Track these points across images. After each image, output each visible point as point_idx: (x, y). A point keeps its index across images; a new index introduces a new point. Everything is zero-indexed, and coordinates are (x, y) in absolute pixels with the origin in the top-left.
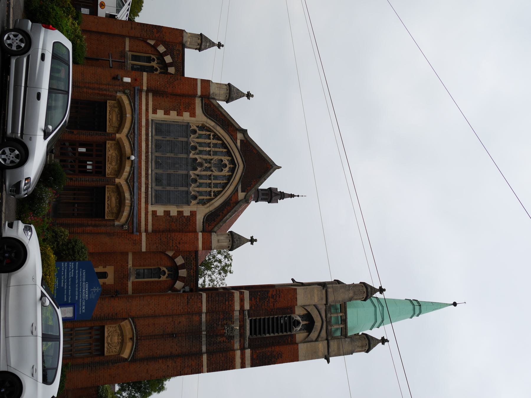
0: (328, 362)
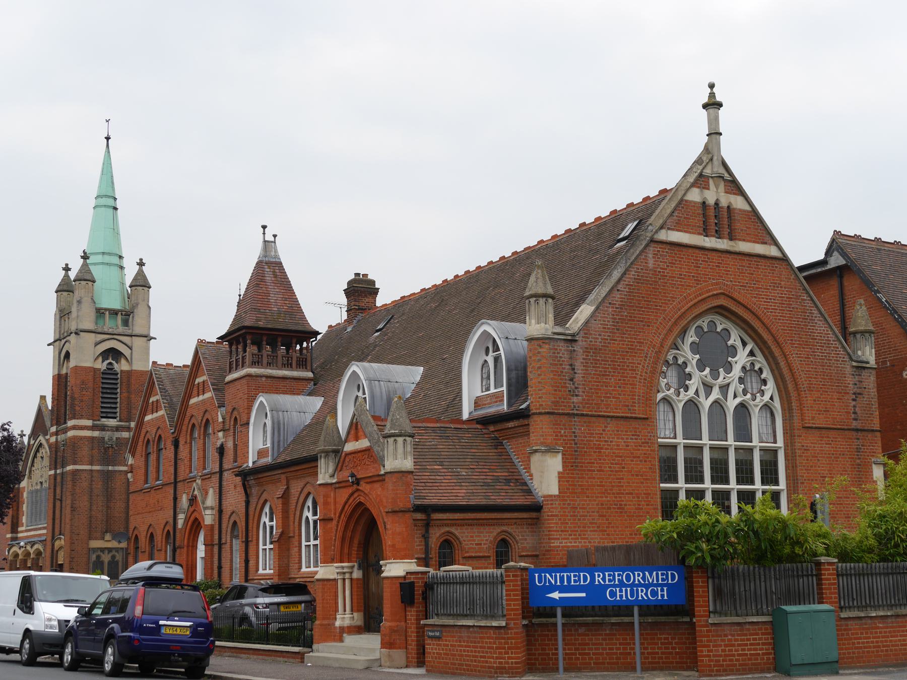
0: (155, 339)
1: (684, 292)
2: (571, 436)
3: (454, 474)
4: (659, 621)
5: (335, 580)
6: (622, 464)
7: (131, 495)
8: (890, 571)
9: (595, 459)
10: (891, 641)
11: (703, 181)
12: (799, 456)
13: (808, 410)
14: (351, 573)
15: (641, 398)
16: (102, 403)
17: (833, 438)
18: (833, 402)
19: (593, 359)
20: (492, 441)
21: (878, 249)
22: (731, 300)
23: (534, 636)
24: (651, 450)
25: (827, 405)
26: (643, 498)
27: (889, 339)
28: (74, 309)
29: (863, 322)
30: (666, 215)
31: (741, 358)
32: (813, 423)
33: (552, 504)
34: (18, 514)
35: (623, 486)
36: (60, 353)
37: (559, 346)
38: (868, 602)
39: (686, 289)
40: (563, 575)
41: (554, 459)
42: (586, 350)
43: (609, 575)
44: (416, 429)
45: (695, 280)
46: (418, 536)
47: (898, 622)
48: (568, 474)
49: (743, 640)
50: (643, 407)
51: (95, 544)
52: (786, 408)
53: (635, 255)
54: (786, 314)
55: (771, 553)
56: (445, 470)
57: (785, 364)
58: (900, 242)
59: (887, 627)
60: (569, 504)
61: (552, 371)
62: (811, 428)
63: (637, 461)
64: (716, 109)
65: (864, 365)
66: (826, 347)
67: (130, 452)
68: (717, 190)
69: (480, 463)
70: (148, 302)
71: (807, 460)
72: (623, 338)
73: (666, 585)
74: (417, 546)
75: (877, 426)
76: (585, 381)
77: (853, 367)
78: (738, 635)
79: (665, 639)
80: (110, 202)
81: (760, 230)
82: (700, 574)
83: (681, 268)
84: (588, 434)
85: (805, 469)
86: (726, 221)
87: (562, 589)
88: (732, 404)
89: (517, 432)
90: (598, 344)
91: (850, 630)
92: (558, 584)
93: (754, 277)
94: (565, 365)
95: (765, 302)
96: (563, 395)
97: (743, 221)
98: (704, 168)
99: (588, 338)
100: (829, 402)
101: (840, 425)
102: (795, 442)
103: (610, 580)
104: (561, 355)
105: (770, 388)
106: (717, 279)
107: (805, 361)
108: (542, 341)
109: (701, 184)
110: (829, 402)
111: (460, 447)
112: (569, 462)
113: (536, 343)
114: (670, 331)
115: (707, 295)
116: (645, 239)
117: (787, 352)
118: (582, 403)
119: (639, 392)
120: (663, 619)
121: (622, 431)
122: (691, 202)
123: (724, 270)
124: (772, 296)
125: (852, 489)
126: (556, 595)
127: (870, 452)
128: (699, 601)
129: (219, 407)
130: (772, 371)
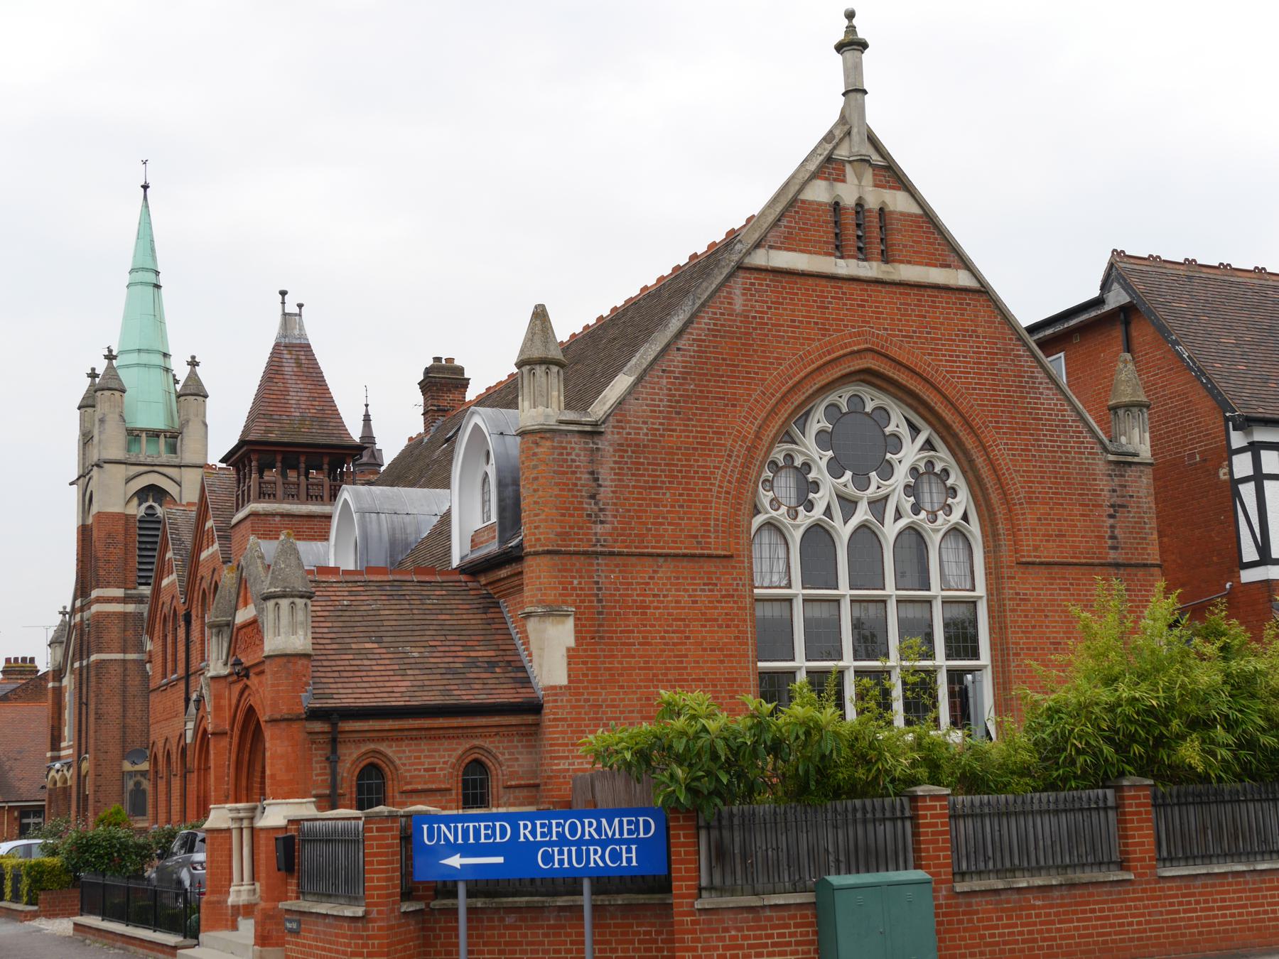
1: (799, 350)
2: (590, 589)
3: (396, 656)
4: (634, 902)
5: (229, 830)
6: (684, 632)
7: (153, 697)
8: (1061, 806)
9: (636, 626)
10: (1059, 930)
11: (833, 169)
12: (1011, 611)
13: (1027, 535)
14: (252, 819)
15: (720, 523)
16: (140, 563)
17: (1073, 579)
18: (1073, 520)
19: (632, 463)
20: (481, 601)
21: (1188, 277)
22: (885, 360)
23: (434, 929)
24: (739, 608)
25: (1062, 525)
26: (722, 686)
27: (1197, 418)
28: (96, 433)
29: (1129, 390)
30: (765, 226)
31: (910, 454)
32: (1035, 557)
33: (556, 701)
34: (60, 723)
35: (686, 668)
36: (84, 495)
37: (571, 443)
38: (1017, 862)
39: (803, 344)
40: (468, 827)
41: (560, 627)
42: (620, 448)
43: (543, 826)
44: (350, 585)
45: (820, 329)
46: (320, 759)
47: (1075, 896)
48: (586, 650)
49: (760, 937)
50: (724, 538)
51: (127, 766)
52: (989, 533)
53: (710, 290)
54: (986, 379)
55: (817, 782)
56: (384, 651)
57: (985, 460)
58: (1264, 269)
59: (1051, 906)
60: (587, 700)
61: (557, 484)
62: (1033, 563)
63: (712, 626)
64: (856, 52)
65: (1130, 459)
66: (1060, 431)
67: (147, 633)
68: (860, 182)
69: (449, 638)
70: (204, 417)
71: (1026, 616)
72: (688, 425)
73: (636, 841)
74: (317, 775)
75: (1153, 555)
76: (618, 498)
77: (1110, 462)
78: (749, 929)
79: (646, 933)
80: (150, 277)
81: (939, 244)
82: (681, 823)
83: (793, 310)
84: (621, 583)
85: (1023, 632)
86: (875, 233)
87: (466, 850)
88: (890, 530)
89: (512, 584)
90: (641, 437)
91: (977, 912)
92: (460, 841)
93: (928, 323)
94: (581, 473)
95: (947, 361)
96: (576, 522)
97: (906, 231)
98: (834, 148)
99: (622, 428)
100: (1065, 520)
101: (1085, 558)
102: (1003, 588)
103: (543, 835)
104: (573, 457)
105: (962, 500)
106: (859, 327)
107: (1020, 455)
108: (539, 435)
109: (829, 174)
110: (1065, 520)
111: (421, 612)
112: (587, 632)
113: (530, 438)
114: (774, 412)
115: (841, 352)
116: (728, 265)
117: (988, 442)
118: (611, 534)
119: (716, 514)
120: (642, 899)
121: (686, 578)
122: (811, 203)
123: (873, 312)
124: (960, 351)
125: (1027, 662)
126: (455, 861)
127: (1140, 601)
128: (679, 870)
129: (224, 563)
130: (964, 473)
